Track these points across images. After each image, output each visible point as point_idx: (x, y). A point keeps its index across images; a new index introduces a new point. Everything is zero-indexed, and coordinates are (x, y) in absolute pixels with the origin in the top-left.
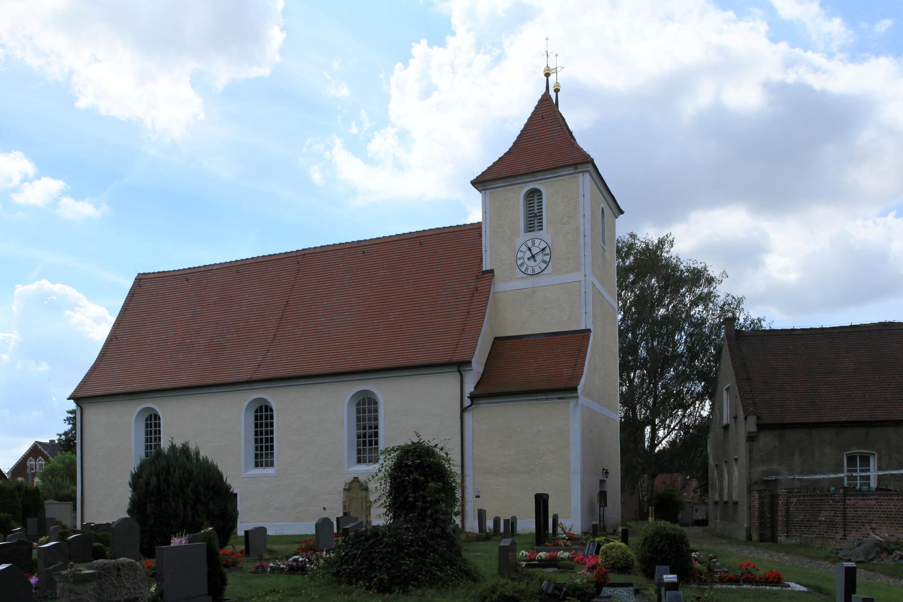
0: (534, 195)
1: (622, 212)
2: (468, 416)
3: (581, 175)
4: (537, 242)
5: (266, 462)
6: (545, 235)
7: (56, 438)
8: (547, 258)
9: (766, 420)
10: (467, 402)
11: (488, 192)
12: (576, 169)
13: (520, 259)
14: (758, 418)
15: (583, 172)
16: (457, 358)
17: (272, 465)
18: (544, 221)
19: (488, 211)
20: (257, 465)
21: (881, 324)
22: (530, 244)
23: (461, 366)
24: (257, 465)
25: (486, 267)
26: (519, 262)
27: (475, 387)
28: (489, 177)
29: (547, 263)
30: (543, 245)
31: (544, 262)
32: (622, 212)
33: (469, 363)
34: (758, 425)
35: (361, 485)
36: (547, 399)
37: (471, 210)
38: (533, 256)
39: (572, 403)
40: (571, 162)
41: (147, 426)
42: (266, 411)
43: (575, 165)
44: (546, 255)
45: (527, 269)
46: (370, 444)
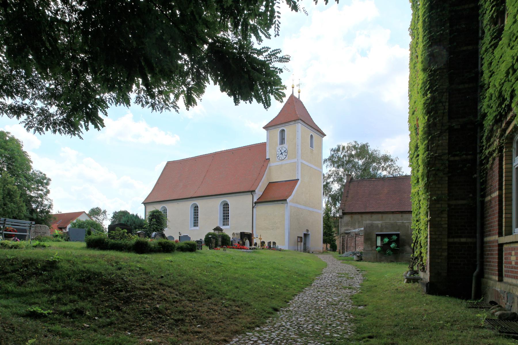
0: (283, 131)
1: (325, 135)
2: (254, 209)
6: (285, 145)
7: (131, 213)
8: (286, 154)
9: (346, 211)
10: (254, 205)
16: (251, 190)
23: (252, 192)
30: (285, 149)
32: (325, 135)
33: (254, 191)
37: (262, 137)
43: (295, 120)
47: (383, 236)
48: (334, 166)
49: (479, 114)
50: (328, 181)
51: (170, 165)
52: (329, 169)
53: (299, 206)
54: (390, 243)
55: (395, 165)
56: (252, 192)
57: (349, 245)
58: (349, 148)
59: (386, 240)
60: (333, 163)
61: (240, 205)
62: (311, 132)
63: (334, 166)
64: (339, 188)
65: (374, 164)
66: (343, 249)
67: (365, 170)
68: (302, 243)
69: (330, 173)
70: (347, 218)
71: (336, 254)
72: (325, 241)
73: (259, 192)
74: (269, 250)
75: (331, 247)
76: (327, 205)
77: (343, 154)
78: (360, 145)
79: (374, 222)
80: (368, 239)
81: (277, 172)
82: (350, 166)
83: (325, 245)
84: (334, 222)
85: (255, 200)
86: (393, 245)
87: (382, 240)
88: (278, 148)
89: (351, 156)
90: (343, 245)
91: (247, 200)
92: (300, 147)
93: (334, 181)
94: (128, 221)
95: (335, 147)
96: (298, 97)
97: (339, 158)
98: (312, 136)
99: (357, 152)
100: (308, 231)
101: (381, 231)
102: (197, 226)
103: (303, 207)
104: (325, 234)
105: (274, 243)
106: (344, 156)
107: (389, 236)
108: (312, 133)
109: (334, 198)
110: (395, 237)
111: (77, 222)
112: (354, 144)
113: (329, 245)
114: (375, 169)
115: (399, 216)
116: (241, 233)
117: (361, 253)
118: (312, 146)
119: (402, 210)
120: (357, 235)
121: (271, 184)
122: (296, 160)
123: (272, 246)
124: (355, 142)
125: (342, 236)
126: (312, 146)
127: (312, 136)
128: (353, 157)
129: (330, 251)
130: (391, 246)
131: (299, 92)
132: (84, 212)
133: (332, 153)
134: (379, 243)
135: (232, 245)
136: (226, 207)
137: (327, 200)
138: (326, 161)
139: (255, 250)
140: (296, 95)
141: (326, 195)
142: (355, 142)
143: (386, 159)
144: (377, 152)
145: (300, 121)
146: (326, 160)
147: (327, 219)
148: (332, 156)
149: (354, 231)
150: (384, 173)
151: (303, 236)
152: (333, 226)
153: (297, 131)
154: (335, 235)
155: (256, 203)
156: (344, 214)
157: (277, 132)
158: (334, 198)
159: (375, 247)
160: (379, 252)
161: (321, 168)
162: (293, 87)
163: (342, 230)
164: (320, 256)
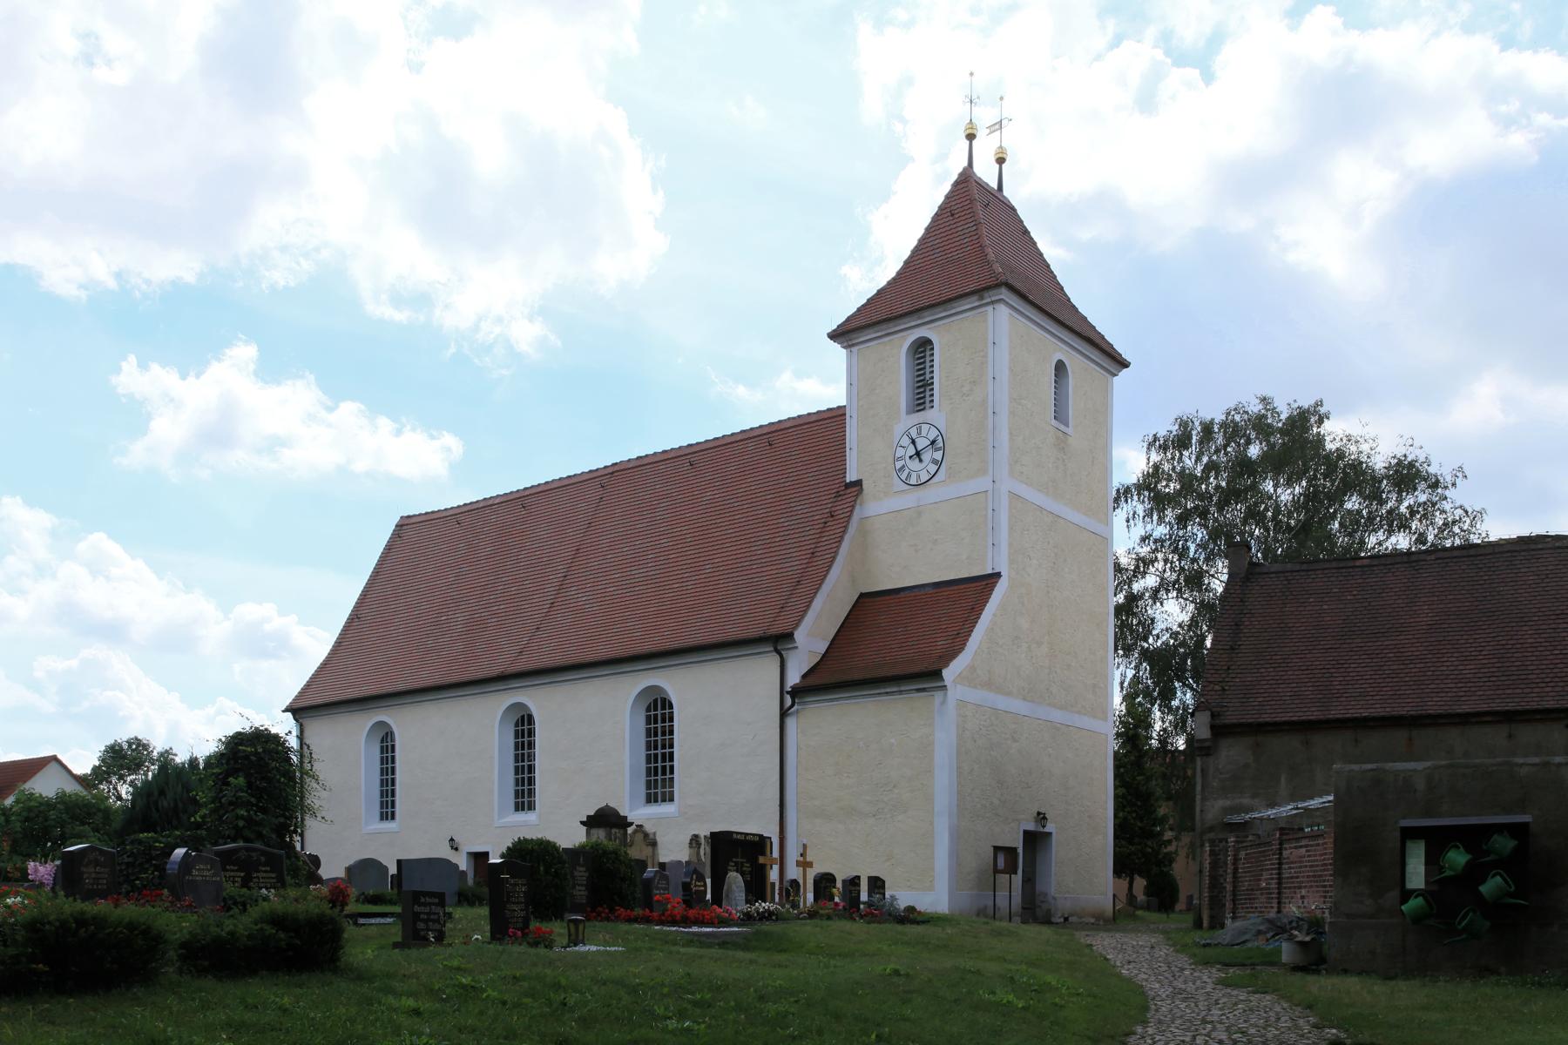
1: (1124, 364)
2: (791, 723)
3: (990, 308)
4: (925, 428)
5: (664, 794)
9: (1230, 718)
10: (788, 701)
11: (855, 349)
12: (982, 298)
13: (900, 458)
14: (1213, 716)
15: (993, 302)
16: (774, 631)
17: (672, 800)
18: (936, 392)
19: (855, 383)
20: (649, 801)
21: (1521, 540)
22: (914, 433)
24: (517, 809)
25: (851, 476)
26: (899, 465)
27: (804, 676)
28: (863, 322)
29: (938, 463)
30: (933, 434)
31: (935, 462)
32: (1124, 364)
33: (789, 636)
34: (1212, 727)
35: (646, 835)
36: (901, 692)
38: (918, 454)
39: (938, 695)
40: (972, 287)
41: (648, 721)
42: (663, 708)
43: (979, 292)
44: (937, 450)
45: (909, 475)
46: (664, 773)
47: (1438, 841)
48: (1161, 520)
49: (1110, 715)
50: (1137, 587)
51: (405, 527)
52: (1139, 530)
53: (1002, 702)
54: (1474, 873)
55: (1447, 506)
56: (780, 641)
57: (1244, 886)
58: (1233, 431)
59: (1457, 858)
60: (1160, 502)
61: (725, 705)
62: (1057, 349)
63: (1161, 520)
64: (1185, 617)
65: (1352, 503)
66: (1216, 903)
67: (1305, 529)
68: (1018, 879)
69: (1144, 551)
70: (1232, 754)
71: (1179, 920)
72: (1123, 866)
73: (811, 642)
74: (847, 925)
75: (1148, 891)
76: (1129, 698)
77: (1205, 459)
78: (1284, 417)
79: (1389, 766)
80: (1361, 851)
81: (902, 537)
82: (1236, 511)
83: (1124, 883)
84: (1164, 776)
85: (793, 679)
86: (1491, 886)
87: (1432, 860)
88: (899, 429)
89: (1244, 466)
90: (1215, 884)
91: (752, 684)
92: (1004, 421)
93: (1164, 585)
94: (162, 793)
95: (1166, 427)
96: (994, 185)
97: (1187, 479)
98: (1060, 368)
99: (1271, 446)
100: (1041, 818)
101: (1428, 814)
102: (531, 807)
103: (1017, 706)
104: (1122, 830)
105: (877, 884)
106: (1211, 467)
107: (1471, 837)
108: (1061, 353)
109: (1165, 666)
110: (1505, 844)
111: (17, 801)
112: (1255, 408)
113: (1140, 883)
114: (1354, 524)
115: (1496, 736)
116: (712, 834)
117: (1315, 925)
118: (1060, 414)
119: (1511, 706)
120: (1289, 831)
121: (867, 604)
122: (983, 483)
123: (864, 897)
124: (1264, 400)
125: (1212, 842)
126: (1060, 414)
127: (1060, 368)
128: (1253, 473)
129: (1148, 908)
130: (1483, 889)
131: (1001, 161)
132: (54, 759)
133: (1155, 457)
134: (1416, 874)
135: (648, 903)
136: (658, 713)
137: (1130, 673)
138: (1124, 494)
139: (767, 927)
140: (986, 172)
141: (1128, 650)
142: (1264, 400)
143: (1406, 475)
144: (1365, 447)
145: (1004, 293)
146: (1127, 490)
147: (1135, 759)
148: (1156, 472)
149: (1271, 812)
150: (1402, 541)
151: (1018, 843)
152: (1159, 792)
153: (991, 345)
154: (1168, 835)
155: (797, 692)
156: (1221, 730)
157: (895, 350)
158: (1165, 666)
159: (1394, 894)
160: (1418, 919)
161: (1108, 523)
162: (971, 137)
163: (1211, 809)
164: (1106, 944)
